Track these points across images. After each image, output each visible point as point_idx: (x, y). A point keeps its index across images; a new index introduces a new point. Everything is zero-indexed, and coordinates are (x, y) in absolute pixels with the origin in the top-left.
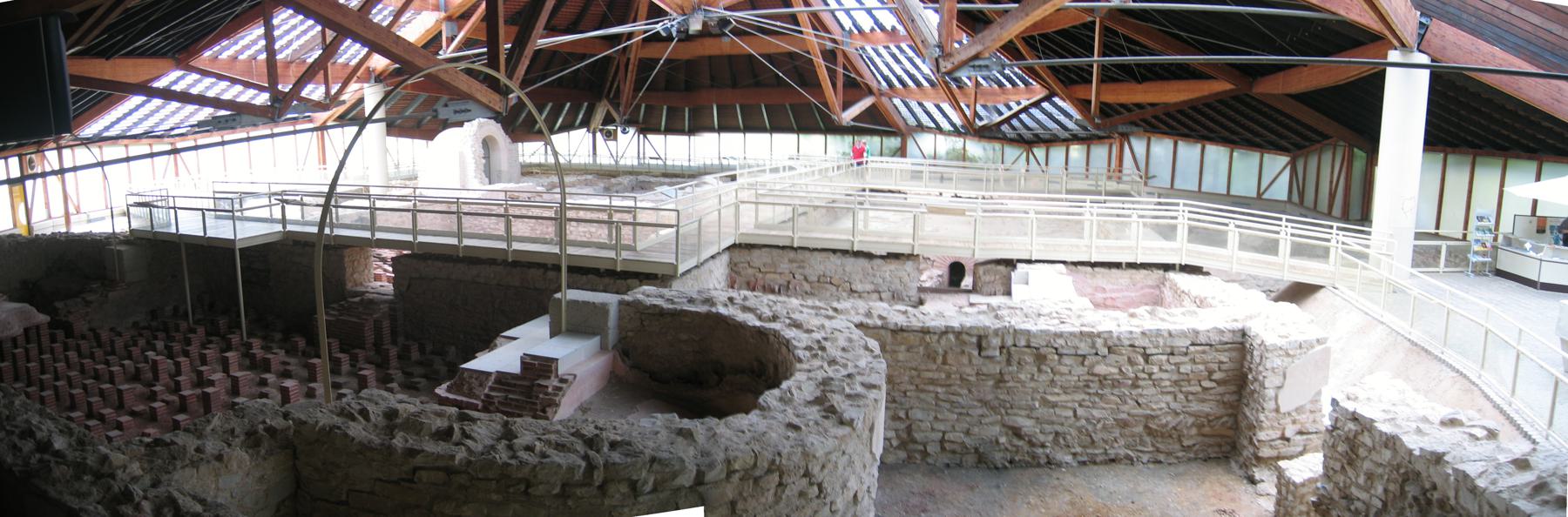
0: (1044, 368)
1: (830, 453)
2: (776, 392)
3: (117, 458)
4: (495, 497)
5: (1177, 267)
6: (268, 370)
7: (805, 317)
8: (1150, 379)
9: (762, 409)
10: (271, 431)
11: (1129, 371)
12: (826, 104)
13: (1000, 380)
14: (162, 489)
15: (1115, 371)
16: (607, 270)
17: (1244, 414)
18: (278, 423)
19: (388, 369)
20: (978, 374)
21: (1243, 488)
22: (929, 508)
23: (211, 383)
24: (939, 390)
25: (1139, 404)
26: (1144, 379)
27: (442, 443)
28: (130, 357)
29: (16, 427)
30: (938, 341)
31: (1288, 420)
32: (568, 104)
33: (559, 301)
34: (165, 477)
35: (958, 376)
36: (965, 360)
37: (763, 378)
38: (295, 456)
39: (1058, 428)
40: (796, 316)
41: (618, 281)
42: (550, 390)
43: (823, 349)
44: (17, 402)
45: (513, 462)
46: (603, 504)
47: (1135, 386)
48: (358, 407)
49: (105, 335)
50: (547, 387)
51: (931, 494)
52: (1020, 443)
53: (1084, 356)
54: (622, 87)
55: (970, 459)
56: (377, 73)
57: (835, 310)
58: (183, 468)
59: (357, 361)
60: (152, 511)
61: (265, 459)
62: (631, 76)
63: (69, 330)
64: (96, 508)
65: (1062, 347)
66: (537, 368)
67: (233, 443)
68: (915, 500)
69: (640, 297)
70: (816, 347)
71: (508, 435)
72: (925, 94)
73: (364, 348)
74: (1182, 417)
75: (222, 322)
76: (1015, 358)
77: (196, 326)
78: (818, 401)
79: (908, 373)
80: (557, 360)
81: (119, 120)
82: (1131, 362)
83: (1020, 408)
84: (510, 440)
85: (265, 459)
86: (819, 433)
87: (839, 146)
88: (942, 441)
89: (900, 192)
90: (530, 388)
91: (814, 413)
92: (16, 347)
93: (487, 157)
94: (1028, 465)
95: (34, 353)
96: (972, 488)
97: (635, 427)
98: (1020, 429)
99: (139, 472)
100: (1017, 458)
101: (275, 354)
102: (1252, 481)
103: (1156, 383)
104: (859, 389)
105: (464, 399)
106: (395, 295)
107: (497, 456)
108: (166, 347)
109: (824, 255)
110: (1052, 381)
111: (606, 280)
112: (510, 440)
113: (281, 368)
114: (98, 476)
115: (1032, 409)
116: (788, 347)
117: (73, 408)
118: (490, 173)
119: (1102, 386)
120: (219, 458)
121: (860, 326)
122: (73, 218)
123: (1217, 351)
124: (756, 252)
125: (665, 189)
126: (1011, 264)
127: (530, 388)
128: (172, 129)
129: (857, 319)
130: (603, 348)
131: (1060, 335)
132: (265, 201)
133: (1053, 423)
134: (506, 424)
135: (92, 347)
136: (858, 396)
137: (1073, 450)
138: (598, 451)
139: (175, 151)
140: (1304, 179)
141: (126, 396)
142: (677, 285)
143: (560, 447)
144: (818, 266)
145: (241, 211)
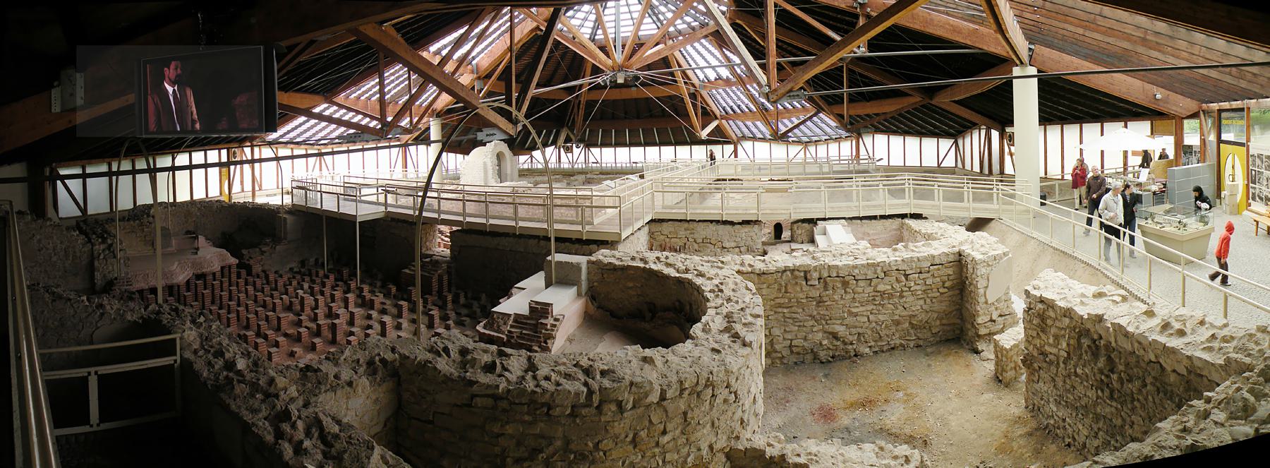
0: (848, 290)
1: (740, 368)
2: (699, 325)
3: (281, 382)
4: (527, 418)
5: (909, 216)
6: (372, 308)
7: (705, 268)
8: (910, 291)
9: (693, 338)
10: (383, 361)
11: (897, 286)
12: (692, 126)
13: (820, 302)
14: (311, 410)
15: (889, 287)
16: (577, 239)
17: (967, 308)
18: (389, 356)
19: (446, 310)
20: (807, 298)
21: (973, 358)
22: (790, 399)
23: (337, 316)
24: (785, 311)
25: (905, 308)
26: (906, 291)
27: (490, 375)
28: (287, 294)
29: (212, 347)
30: (781, 277)
31: (993, 308)
32: (545, 131)
33: (550, 261)
34: (313, 400)
35: (795, 300)
36: (798, 289)
37: (683, 313)
38: (399, 384)
39: (860, 331)
40: (700, 268)
41: (584, 246)
42: (549, 327)
43: (721, 291)
44: (214, 327)
45: (538, 390)
46: (600, 420)
47: (901, 297)
48: (442, 346)
49: (272, 277)
50: (547, 324)
51: (790, 389)
52: (839, 343)
53: (871, 280)
54: (576, 119)
55: (809, 357)
56: (438, 111)
57: (722, 262)
58: (326, 392)
59: (427, 304)
60: (304, 429)
61: (380, 385)
62: (582, 112)
63: (249, 269)
64: (264, 424)
65: (858, 275)
66: (540, 311)
67: (359, 371)
68: (781, 394)
69: (601, 257)
70: (717, 290)
71: (532, 367)
72: (747, 116)
73: (431, 295)
74: (930, 314)
75: (346, 272)
76: (831, 285)
77: (329, 274)
78: (727, 330)
79: (769, 303)
80: (552, 304)
81: (289, 132)
82: (898, 281)
83: (836, 319)
84: (534, 372)
85: (380, 385)
86: (732, 354)
87: (700, 152)
88: (791, 346)
89: (739, 180)
90: (536, 326)
91: (726, 338)
92: (214, 280)
93: (499, 165)
94: (843, 358)
95: (226, 285)
96: (814, 378)
97: (614, 357)
98: (837, 333)
99: (295, 394)
100: (836, 354)
101: (377, 296)
102: (977, 352)
103: (913, 293)
104: (750, 319)
105: (496, 334)
106: (451, 258)
107: (527, 385)
108: (310, 287)
109: (705, 224)
110: (854, 298)
111: (577, 246)
112: (534, 372)
113: (380, 307)
114: (267, 395)
115: (844, 319)
116: (698, 291)
117: (247, 327)
118: (501, 176)
119: (883, 299)
120: (350, 384)
121: (738, 272)
122: (257, 193)
123: (946, 267)
124: (665, 224)
125: (608, 182)
126: (813, 222)
127: (536, 326)
128: (320, 140)
129: (737, 268)
130: (579, 295)
131: (855, 267)
132: (374, 191)
133: (856, 327)
134: (529, 358)
135: (263, 284)
136: (750, 323)
137: (869, 345)
138: (593, 379)
139: (320, 155)
140: (964, 152)
141: (283, 322)
142: (620, 247)
143: (568, 376)
144: (703, 232)
145: (360, 197)
